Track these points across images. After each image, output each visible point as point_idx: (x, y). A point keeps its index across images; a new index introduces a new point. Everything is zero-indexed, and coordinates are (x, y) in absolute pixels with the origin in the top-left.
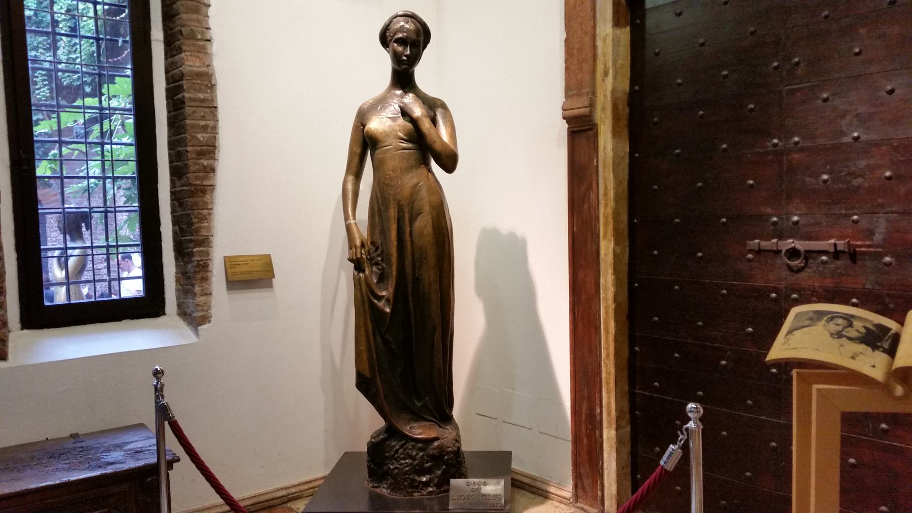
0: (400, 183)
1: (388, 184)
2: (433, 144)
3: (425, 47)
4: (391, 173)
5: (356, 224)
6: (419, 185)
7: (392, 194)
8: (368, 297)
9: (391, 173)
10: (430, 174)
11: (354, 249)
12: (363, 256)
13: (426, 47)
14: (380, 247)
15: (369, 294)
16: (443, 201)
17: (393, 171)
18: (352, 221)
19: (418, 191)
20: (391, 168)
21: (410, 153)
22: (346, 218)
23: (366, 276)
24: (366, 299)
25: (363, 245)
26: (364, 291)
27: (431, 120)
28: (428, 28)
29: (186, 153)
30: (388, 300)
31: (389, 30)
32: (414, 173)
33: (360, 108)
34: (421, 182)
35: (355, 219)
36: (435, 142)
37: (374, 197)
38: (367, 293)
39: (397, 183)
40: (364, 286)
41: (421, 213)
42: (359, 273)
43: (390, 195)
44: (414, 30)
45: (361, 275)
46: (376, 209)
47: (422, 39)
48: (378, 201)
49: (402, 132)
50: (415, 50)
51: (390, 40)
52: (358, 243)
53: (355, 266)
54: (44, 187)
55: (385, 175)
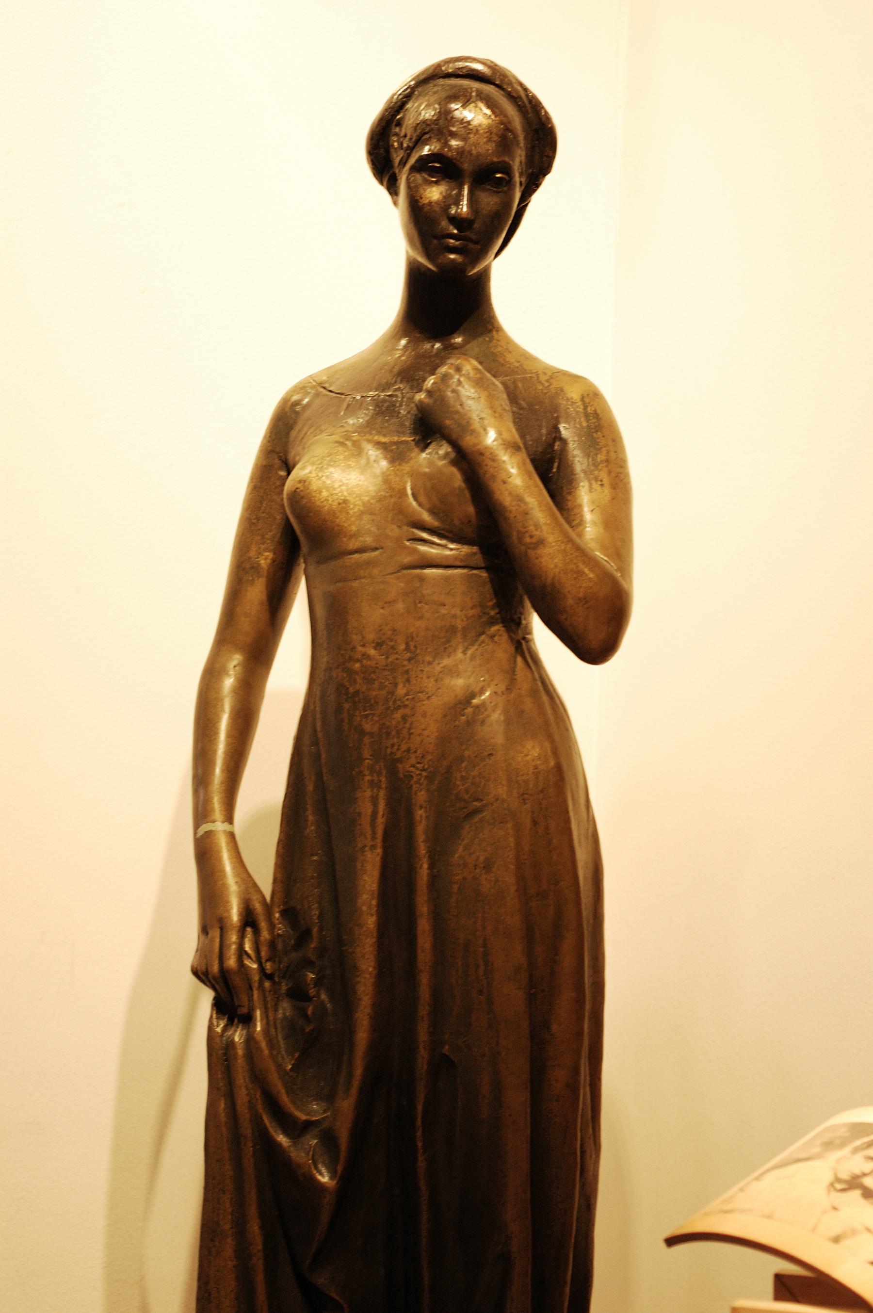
0: (401, 691)
1: (357, 692)
2: (531, 553)
3: (532, 184)
4: (372, 652)
5: (232, 836)
6: (475, 701)
7: (371, 734)
8: (257, 1121)
9: (372, 652)
10: (519, 660)
11: (215, 934)
12: (247, 962)
13: (538, 186)
14: (315, 930)
15: (260, 1108)
16: (565, 768)
17: (378, 645)
18: (219, 827)
19: (468, 723)
20: (371, 636)
21: (447, 579)
22: (201, 814)
23: (250, 1040)
24: (247, 1129)
25: (249, 920)
26: (242, 1096)
27: (533, 461)
28: (548, 119)
29: (516, 519)
30: (329, 1139)
31: (399, 124)
32: (459, 655)
33: (285, 401)
34: (482, 692)
35: (229, 818)
36: (541, 542)
37: (307, 740)
38: (251, 1106)
39: (392, 693)
40: (241, 1078)
41: (477, 811)
42: (230, 1023)
43: (362, 733)
44: (489, 130)
45: (238, 1036)
46: (310, 788)
47: (518, 160)
48: (318, 756)
49: (422, 498)
50: (489, 201)
51: (403, 162)
52: (235, 915)
53: (215, 999)
54: (418, 344)
55: (351, 659)
